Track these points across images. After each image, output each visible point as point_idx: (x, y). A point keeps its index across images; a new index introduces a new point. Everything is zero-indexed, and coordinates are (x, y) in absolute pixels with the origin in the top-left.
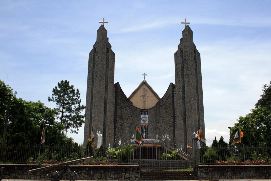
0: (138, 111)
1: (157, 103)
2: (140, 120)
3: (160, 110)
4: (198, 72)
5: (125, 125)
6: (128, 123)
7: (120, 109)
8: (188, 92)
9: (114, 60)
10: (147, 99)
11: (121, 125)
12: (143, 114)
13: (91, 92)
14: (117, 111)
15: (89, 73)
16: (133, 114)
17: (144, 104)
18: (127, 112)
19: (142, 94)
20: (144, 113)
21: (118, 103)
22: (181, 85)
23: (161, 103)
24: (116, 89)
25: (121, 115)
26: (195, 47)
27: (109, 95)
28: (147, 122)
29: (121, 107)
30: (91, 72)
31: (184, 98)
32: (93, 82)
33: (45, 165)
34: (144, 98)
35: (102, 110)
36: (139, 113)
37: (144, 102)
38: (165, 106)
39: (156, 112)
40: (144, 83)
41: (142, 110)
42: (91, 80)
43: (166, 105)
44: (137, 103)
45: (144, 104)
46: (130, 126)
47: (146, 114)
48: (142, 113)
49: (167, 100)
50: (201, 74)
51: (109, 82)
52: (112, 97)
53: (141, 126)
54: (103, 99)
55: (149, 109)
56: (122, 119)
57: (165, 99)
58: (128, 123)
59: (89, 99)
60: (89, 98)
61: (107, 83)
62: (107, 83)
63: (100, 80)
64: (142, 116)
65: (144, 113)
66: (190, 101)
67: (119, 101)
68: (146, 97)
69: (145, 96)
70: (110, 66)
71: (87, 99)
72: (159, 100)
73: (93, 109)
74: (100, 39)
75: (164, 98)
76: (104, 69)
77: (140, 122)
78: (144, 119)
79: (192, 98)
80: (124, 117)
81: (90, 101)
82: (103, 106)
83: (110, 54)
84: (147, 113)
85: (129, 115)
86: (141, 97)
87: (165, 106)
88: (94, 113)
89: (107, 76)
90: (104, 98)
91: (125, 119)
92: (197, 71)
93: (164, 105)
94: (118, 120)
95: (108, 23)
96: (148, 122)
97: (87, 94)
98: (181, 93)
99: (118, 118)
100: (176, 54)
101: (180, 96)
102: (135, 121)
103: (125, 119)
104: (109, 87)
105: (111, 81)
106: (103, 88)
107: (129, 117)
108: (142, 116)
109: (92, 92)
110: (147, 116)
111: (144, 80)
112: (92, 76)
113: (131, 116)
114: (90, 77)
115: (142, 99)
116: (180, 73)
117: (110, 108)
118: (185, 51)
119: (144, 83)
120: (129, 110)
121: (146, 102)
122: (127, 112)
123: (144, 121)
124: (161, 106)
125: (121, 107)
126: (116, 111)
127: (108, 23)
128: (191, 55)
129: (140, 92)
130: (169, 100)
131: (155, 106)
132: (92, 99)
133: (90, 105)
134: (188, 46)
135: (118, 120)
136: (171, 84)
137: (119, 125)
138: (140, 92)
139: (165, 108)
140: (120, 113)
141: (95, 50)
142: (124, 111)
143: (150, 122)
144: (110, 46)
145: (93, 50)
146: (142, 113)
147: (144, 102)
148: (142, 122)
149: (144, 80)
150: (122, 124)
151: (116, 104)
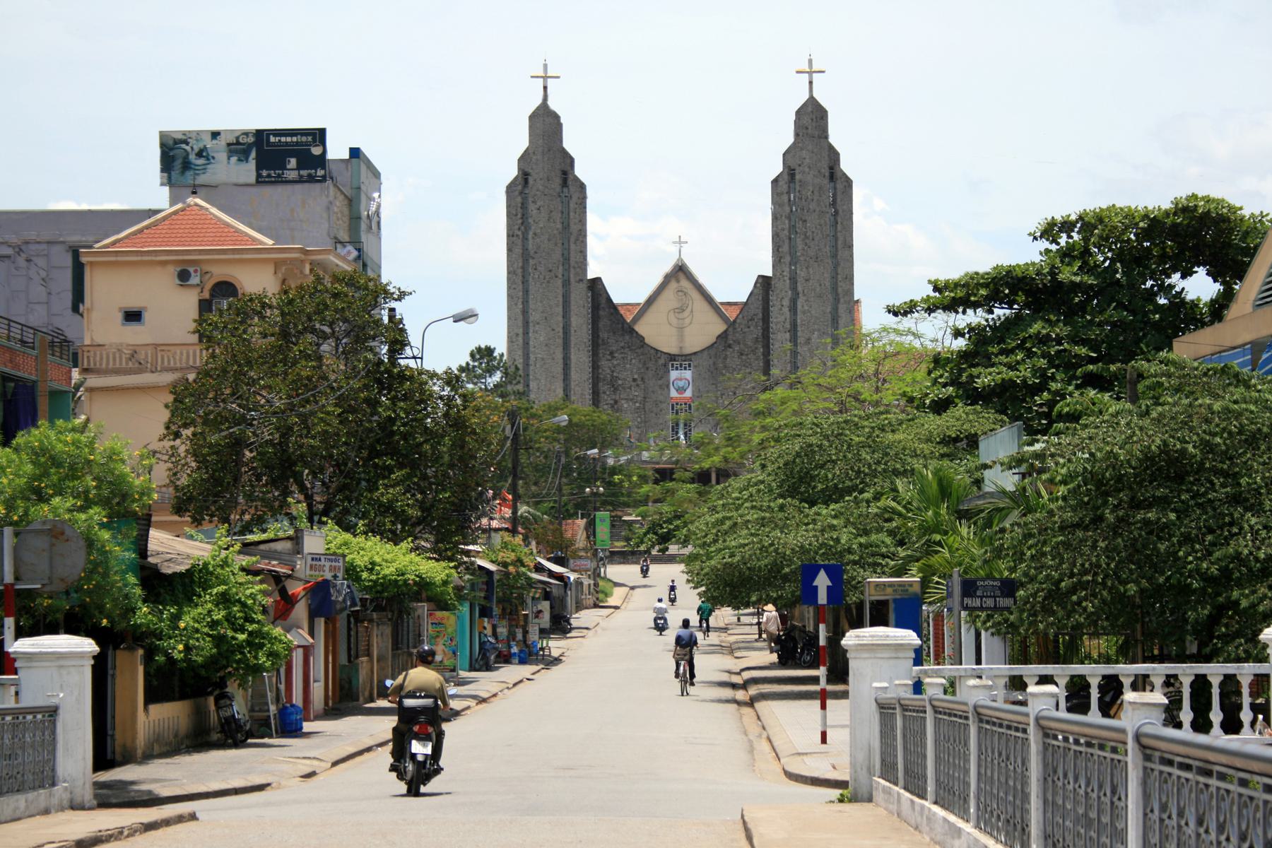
0: (662, 361)
1: (719, 337)
2: (668, 386)
3: (725, 358)
4: (840, 242)
5: (625, 406)
6: (631, 400)
7: (609, 357)
8: (804, 313)
9: (585, 208)
10: (687, 321)
11: (612, 407)
12: (677, 369)
13: (523, 315)
14: (598, 367)
15: (509, 250)
16: (647, 369)
17: (681, 337)
18: (628, 366)
19: (675, 304)
20: (681, 365)
21: (600, 341)
22: (788, 286)
23: (730, 337)
24: (592, 296)
25: (612, 376)
26: (834, 156)
27: (575, 321)
28: (688, 393)
29: (611, 353)
30: (518, 250)
31: (794, 326)
32: (525, 281)
33: (264, 536)
34: (680, 316)
35: (558, 369)
36: (665, 365)
37: (681, 329)
38: (742, 346)
39: (714, 363)
40: (680, 271)
41: (672, 357)
42: (521, 278)
43: (745, 345)
44: (659, 333)
45: (681, 337)
46: (638, 408)
47: (685, 369)
48: (673, 365)
49: (746, 330)
50: (850, 247)
51: (572, 280)
52: (585, 326)
53: (673, 405)
54: (559, 337)
55: (695, 353)
56: (616, 389)
57: (740, 324)
58: (631, 400)
59: (517, 335)
60: (516, 331)
61: (566, 283)
62: (566, 283)
63: (548, 282)
64: (674, 374)
65: (681, 365)
66: (808, 341)
67: (603, 335)
68: (686, 313)
69: (684, 310)
70: (574, 228)
71: (509, 332)
72: (726, 323)
73: (531, 368)
74: (540, 149)
75: (738, 321)
76: (556, 245)
77: (669, 393)
78: (681, 384)
79: (814, 330)
80: (620, 382)
81: (520, 339)
82: (559, 355)
83: (619, 308)
84: (690, 365)
85: (636, 376)
86: (672, 313)
87: (742, 346)
88: (536, 379)
89: (566, 259)
90: (561, 334)
91: (624, 388)
92: (836, 240)
93: (739, 343)
94: (604, 393)
95: (558, 77)
96: (693, 392)
97: (509, 318)
98: (786, 310)
99: (603, 387)
100: (775, 182)
101: (782, 318)
102: (653, 392)
103: (624, 388)
104: (573, 296)
105: (578, 278)
106: (557, 306)
107: (634, 380)
108: (674, 374)
109: (525, 312)
110: (688, 374)
111: (680, 259)
112: (520, 264)
113: (642, 379)
114: (515, 266)
115: (674, 321)
116: (785, 248)
117: (581, 358)
118: (800, 181)
119: (680, 271)
120: (633, 361)
121: (687, 331)
122: (628, 366)
123: (681, 390)
124: (730, 346)
125: (611, 353)
126: (595, 366)
127: (558, 77)
128: (815, 198)
129: (669, 297)
130: (752, 328)
131: (713, 345)
132: (526, 333)
133: (520, 352)
134: (809, 167)
135: (604, 393)
136: (760, 280)
137: (606, 407)
138: (669, 299)
139: (742, 354)
140: (608, 371)
141: (526, 181)
142: (618, 365)
143: (698, 394)
144: (569, 161)
145: (520, 179)
146: (673, 365)
147: (681, 329)
148: (674, 393)
149: (680, 259)
150: (616, 402)
151: (596, 344)
